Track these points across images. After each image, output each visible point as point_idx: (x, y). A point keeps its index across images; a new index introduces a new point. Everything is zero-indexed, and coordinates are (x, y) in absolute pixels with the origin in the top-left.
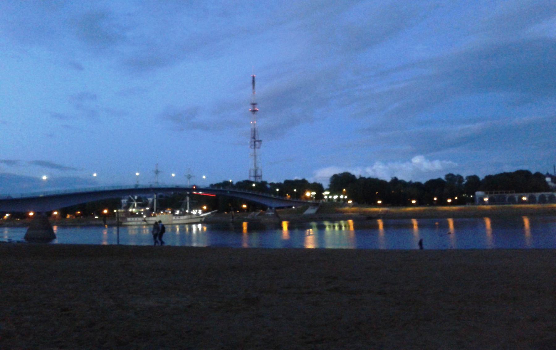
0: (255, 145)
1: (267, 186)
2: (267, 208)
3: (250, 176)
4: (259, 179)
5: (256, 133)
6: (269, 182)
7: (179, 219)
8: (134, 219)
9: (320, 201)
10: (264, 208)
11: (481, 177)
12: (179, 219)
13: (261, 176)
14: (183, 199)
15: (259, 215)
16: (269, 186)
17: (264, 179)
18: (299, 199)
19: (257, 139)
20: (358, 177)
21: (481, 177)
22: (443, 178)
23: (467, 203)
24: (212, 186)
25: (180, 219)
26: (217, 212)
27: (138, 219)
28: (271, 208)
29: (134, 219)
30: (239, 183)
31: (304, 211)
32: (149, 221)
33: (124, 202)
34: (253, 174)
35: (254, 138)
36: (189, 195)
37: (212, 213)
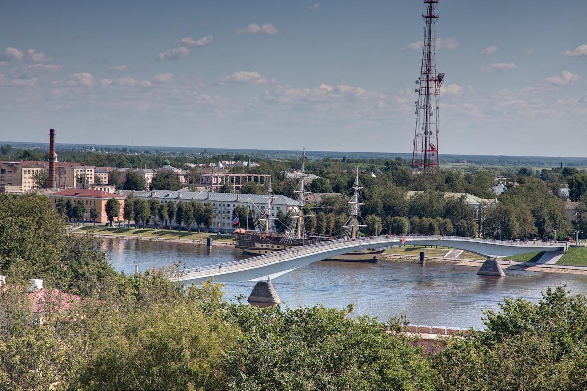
34: (420, 145)
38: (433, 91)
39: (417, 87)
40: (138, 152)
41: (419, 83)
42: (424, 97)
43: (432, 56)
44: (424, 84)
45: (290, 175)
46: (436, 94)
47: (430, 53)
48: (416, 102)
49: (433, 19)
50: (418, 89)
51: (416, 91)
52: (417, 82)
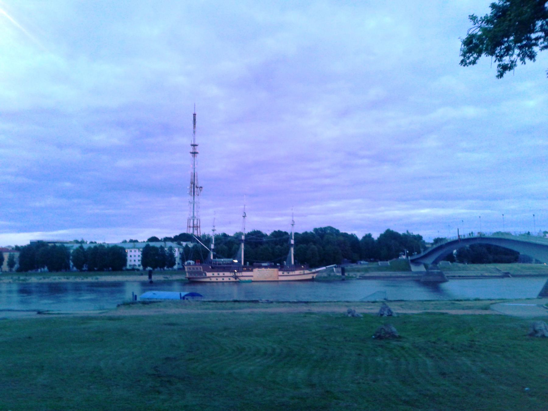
22: (312, 231)
49: (195, 154)
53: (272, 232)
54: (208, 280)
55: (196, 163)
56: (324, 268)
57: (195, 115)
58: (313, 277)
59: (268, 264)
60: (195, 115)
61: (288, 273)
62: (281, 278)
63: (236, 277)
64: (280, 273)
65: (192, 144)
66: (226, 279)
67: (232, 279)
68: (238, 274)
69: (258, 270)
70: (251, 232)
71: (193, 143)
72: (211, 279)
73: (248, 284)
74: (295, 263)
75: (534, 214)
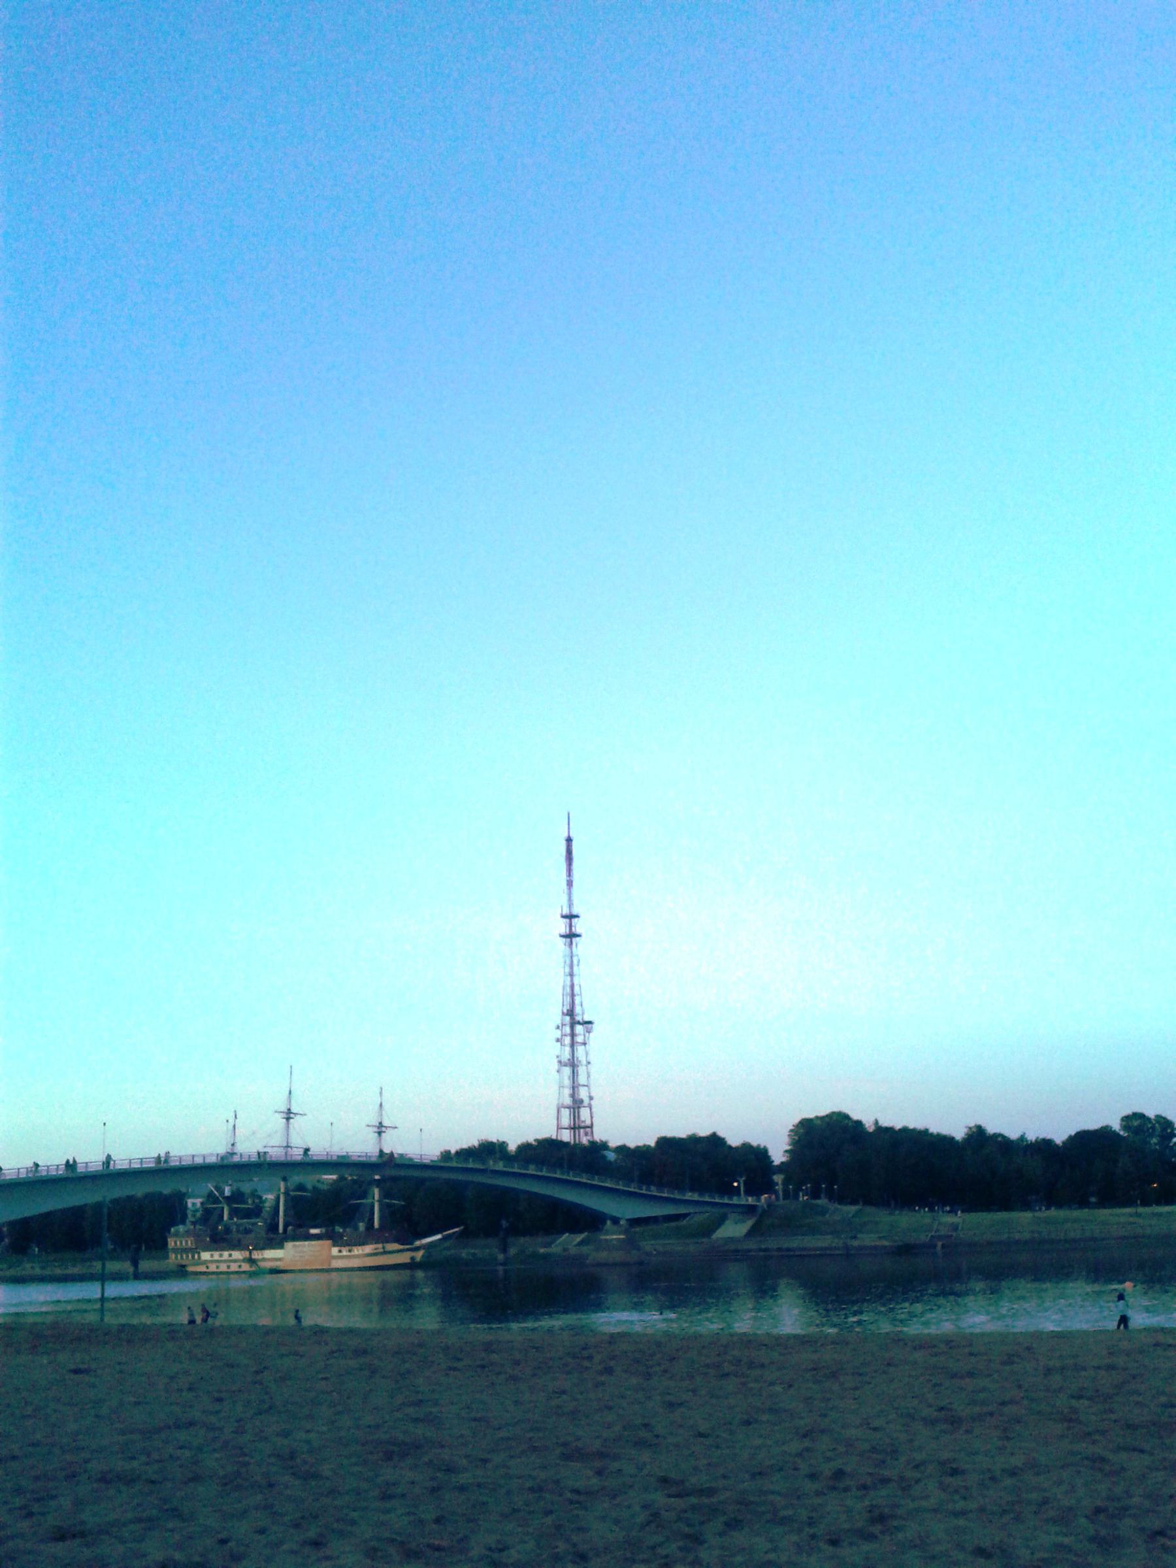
0: (573, 1035)
1: (604, 1157)
2: (604, 1223)
3: (559, 1128)
4: (586, 1134)
5: (577, 1000)
6: (613, 1144)
7: (348, 1254)
8: (221, 1256)
9: (759, 1200)
10: (592, 1222)
11: (453, 1151)
12: (348, 1254)
13: (591, 1127)
14: (364, 1195)
15: (581, 1243)
16: (611, 1156)
17: (599, 1135)
18: (735, 1198)
19: (579, 1018)
20: (869, 1126)
21: (453, 1151)
22: (1116, 1126)
23: (167, 1234)
24: (446, 1155)
25: (352, 1253)
26: (461, 1235)
27: (230, 1255)
28: (615, 1221)
29: (221, 1256)
30: (525, 1148)
31: (714, 1231)
32: (264, 1260)
33: (194, 1204)
34: (566, 1120)
35: (571, 1013)
36: (378, 1183)
37: (444, 1239)
38: (579, 1039)
39: (558, 1034)
40: (881, 1303)
41: (560, 1028)
42: (568, 1049)
43: (577, 989)
44: (567, 1030)
45: (1172, 1473)
46: (585, 1044)
47: (572, 986)
48: (558, 1057)
49: (574, 940)
50: (559, 1037)
51: (558, 1040)
52: (558, 1027)
53: (727, 1139)
54: (203, 1269)
55: (575, 962)
56: (439, 1237)
57: (569, 840)
58: (413, 1258)
59: (321, 1231)
60: (569, 840)
61: (350, 1251)
62: (337, 1264)
63: (251, 1261)
64: (335, 1251)
65: (564, 913)
66: (234, 1267)
67: (246, 1267)
68: (256, 1255)
69: (294, 1246)
70: (967, 1134)
71: (566, 911)
72: (207, 1267)
73: (299, 1277)
74: (381, 1225)
75: (423, 1128)
